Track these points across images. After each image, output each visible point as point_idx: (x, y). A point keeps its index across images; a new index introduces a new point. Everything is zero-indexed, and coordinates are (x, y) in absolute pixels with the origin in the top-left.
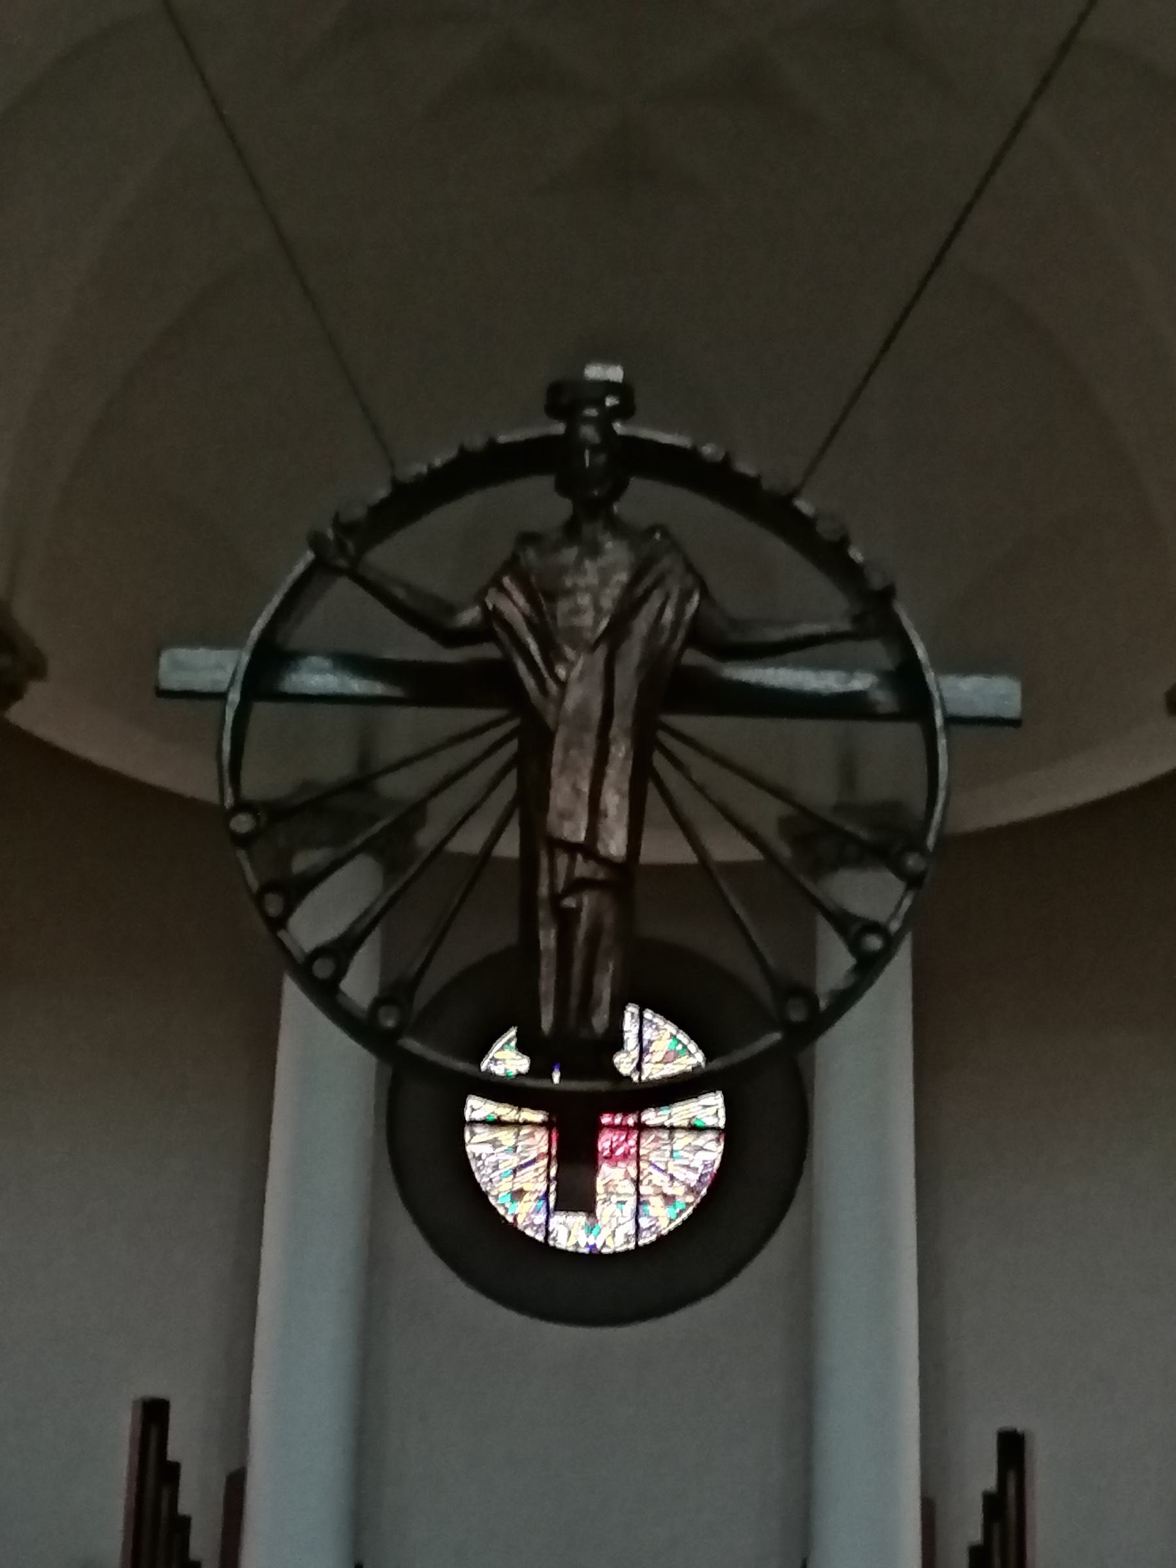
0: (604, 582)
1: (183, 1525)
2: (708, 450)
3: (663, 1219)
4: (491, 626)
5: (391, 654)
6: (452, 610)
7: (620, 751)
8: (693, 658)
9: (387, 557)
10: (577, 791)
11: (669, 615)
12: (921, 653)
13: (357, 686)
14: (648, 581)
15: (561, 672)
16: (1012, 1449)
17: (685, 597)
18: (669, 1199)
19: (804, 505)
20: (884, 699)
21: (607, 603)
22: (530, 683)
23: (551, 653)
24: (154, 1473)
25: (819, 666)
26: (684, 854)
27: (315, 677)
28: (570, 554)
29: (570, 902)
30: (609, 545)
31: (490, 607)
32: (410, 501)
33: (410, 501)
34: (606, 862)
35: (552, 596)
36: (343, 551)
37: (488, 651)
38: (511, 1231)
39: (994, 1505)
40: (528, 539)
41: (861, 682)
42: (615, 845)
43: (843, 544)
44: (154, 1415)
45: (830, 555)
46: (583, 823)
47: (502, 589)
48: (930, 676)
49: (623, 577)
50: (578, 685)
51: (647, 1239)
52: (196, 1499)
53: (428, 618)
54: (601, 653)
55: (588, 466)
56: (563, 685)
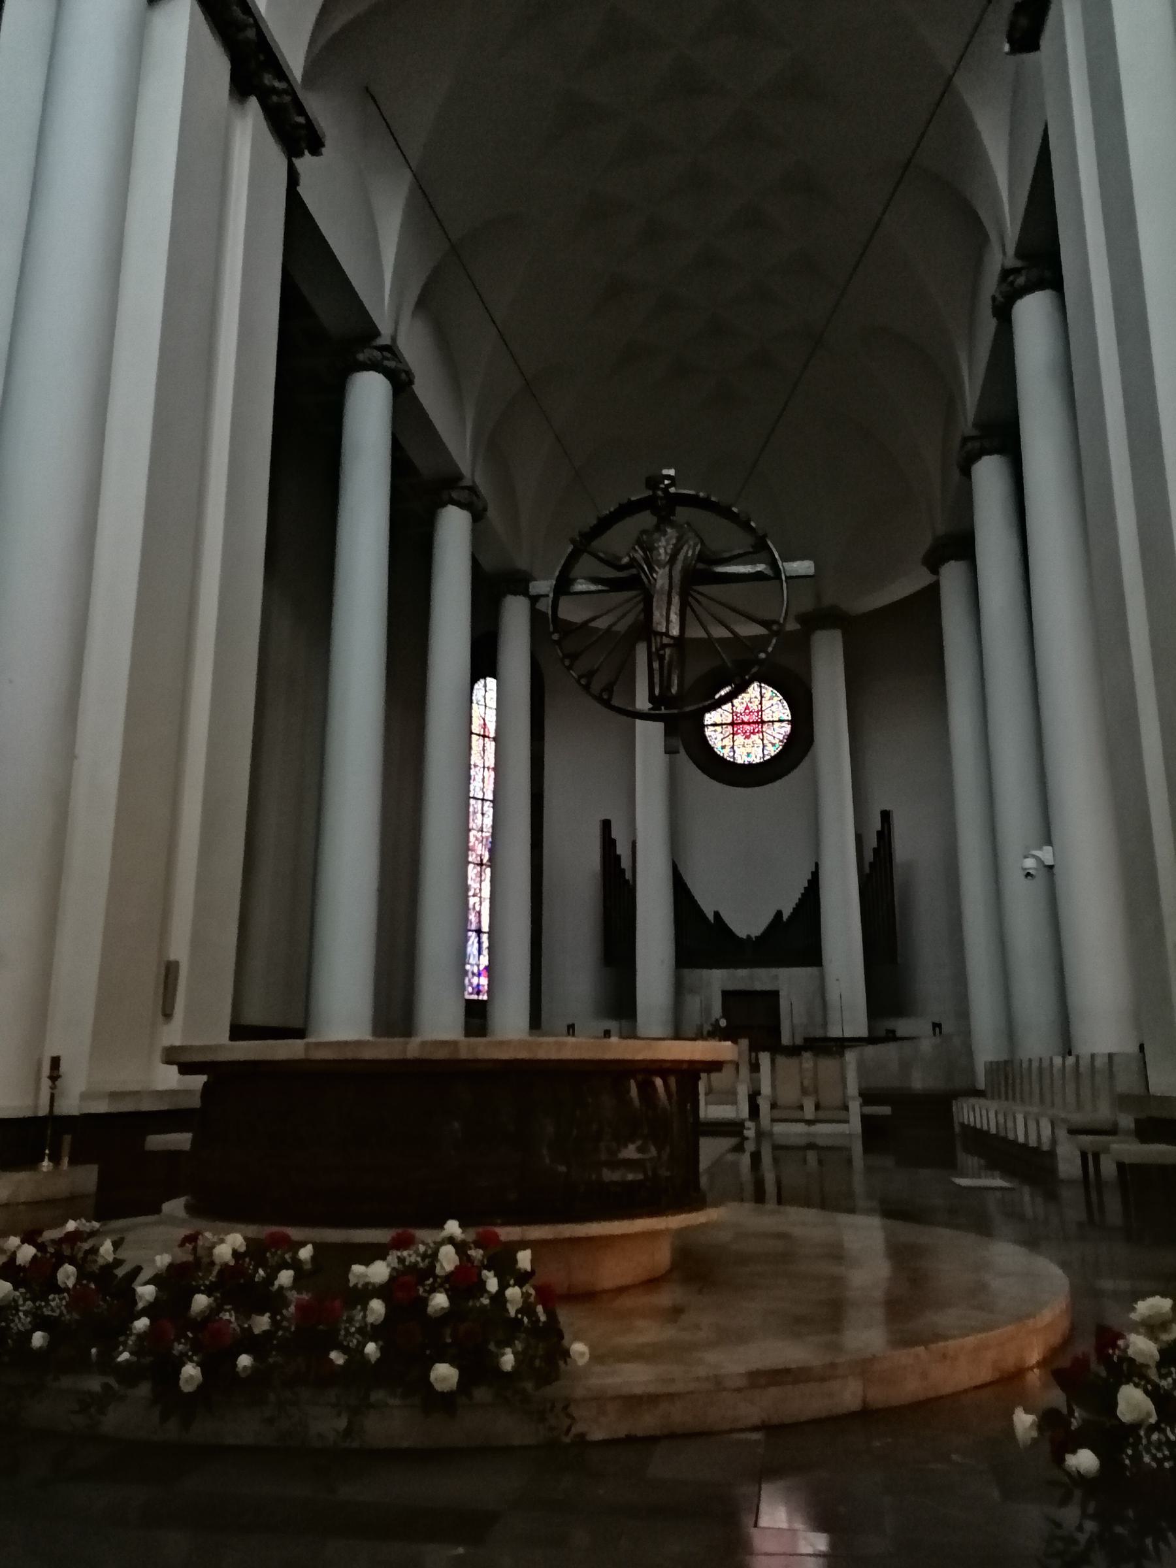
0: (668, 544)
1: (618, 858)
2: (701, 494)
3: (772, 751)
4: (633, 563)
5: (602, 576)
6: (620, 559)
7: (676, 600)
8: (700, 566)
12: (777, 556)
13: (593, 588)
16: (886, 816)
17: (695, 545)
18: (774, 745)
19: (735, 509)
20: (769, 572)
21: (669, 551)
22: (645, 580)
23: (652, 570)
24: (608, 844)
25: (745, 563)
26: (702, 634)
27: (581, 586)
28: (656, 535)
29: (662, 652)
30: (669, 530)
32: (604, 524)
33: (604, 524)
34: (672, 637)
35: (651, 551)
36: (584, 543)
37: (634, 571)
38: (722, 759)
39: (880, 834)
40: (644, 532)
41: (761, 567)
42: (675, 631)
43: (749, 521)
44: (606, 825)
48: (780, 563)
49: (674, 541)
50: (661, 578)
51: (767, 758)
52: (622, 849)
53: (613, 563)
54: (667, 569)
55: (663, 506)
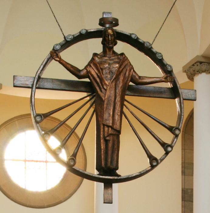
9: (65, 55)
10: (110, 114)
11: (127, 73)
14: (123, 67)
15: (105, 87)
31: (88, 70)
33: (67, 44)
36: (54, 55)
45: (160, 62)
46: (111, 122)
47: (90, 66)
53: (73, 70)
56: (106, 90)
